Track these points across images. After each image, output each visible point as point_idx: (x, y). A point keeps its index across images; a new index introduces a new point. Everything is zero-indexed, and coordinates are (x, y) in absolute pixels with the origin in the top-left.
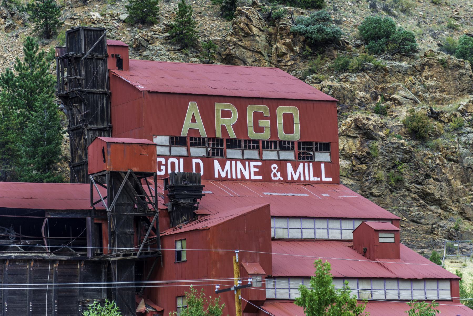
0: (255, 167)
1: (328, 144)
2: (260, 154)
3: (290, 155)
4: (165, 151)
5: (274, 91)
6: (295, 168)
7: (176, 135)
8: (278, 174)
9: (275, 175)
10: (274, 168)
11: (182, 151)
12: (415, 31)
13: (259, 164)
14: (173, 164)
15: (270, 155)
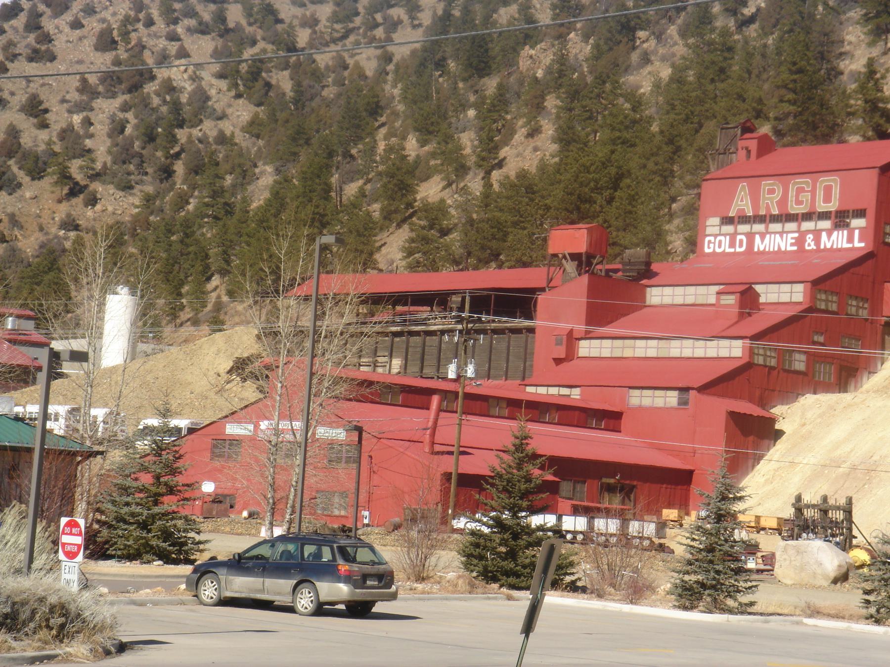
0: (792, 238)
1: (865, 210)
2: (799, 226)
3: (826, 224)
4: (716, 230)
5: (749, 610)
6: (829, 235)
7: (725, 215)
8: (812, 244)
9: (809, 245)
10: (810, 237)
11: (729, 229)
12: (411, 589)
13: (796, 235)
14: (720, 242)
15: (807, 225)
